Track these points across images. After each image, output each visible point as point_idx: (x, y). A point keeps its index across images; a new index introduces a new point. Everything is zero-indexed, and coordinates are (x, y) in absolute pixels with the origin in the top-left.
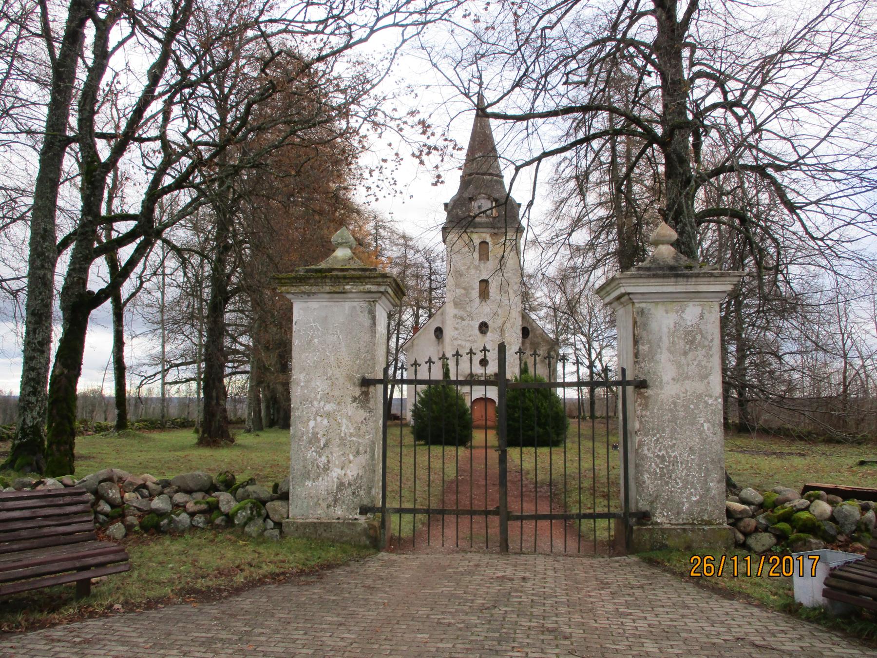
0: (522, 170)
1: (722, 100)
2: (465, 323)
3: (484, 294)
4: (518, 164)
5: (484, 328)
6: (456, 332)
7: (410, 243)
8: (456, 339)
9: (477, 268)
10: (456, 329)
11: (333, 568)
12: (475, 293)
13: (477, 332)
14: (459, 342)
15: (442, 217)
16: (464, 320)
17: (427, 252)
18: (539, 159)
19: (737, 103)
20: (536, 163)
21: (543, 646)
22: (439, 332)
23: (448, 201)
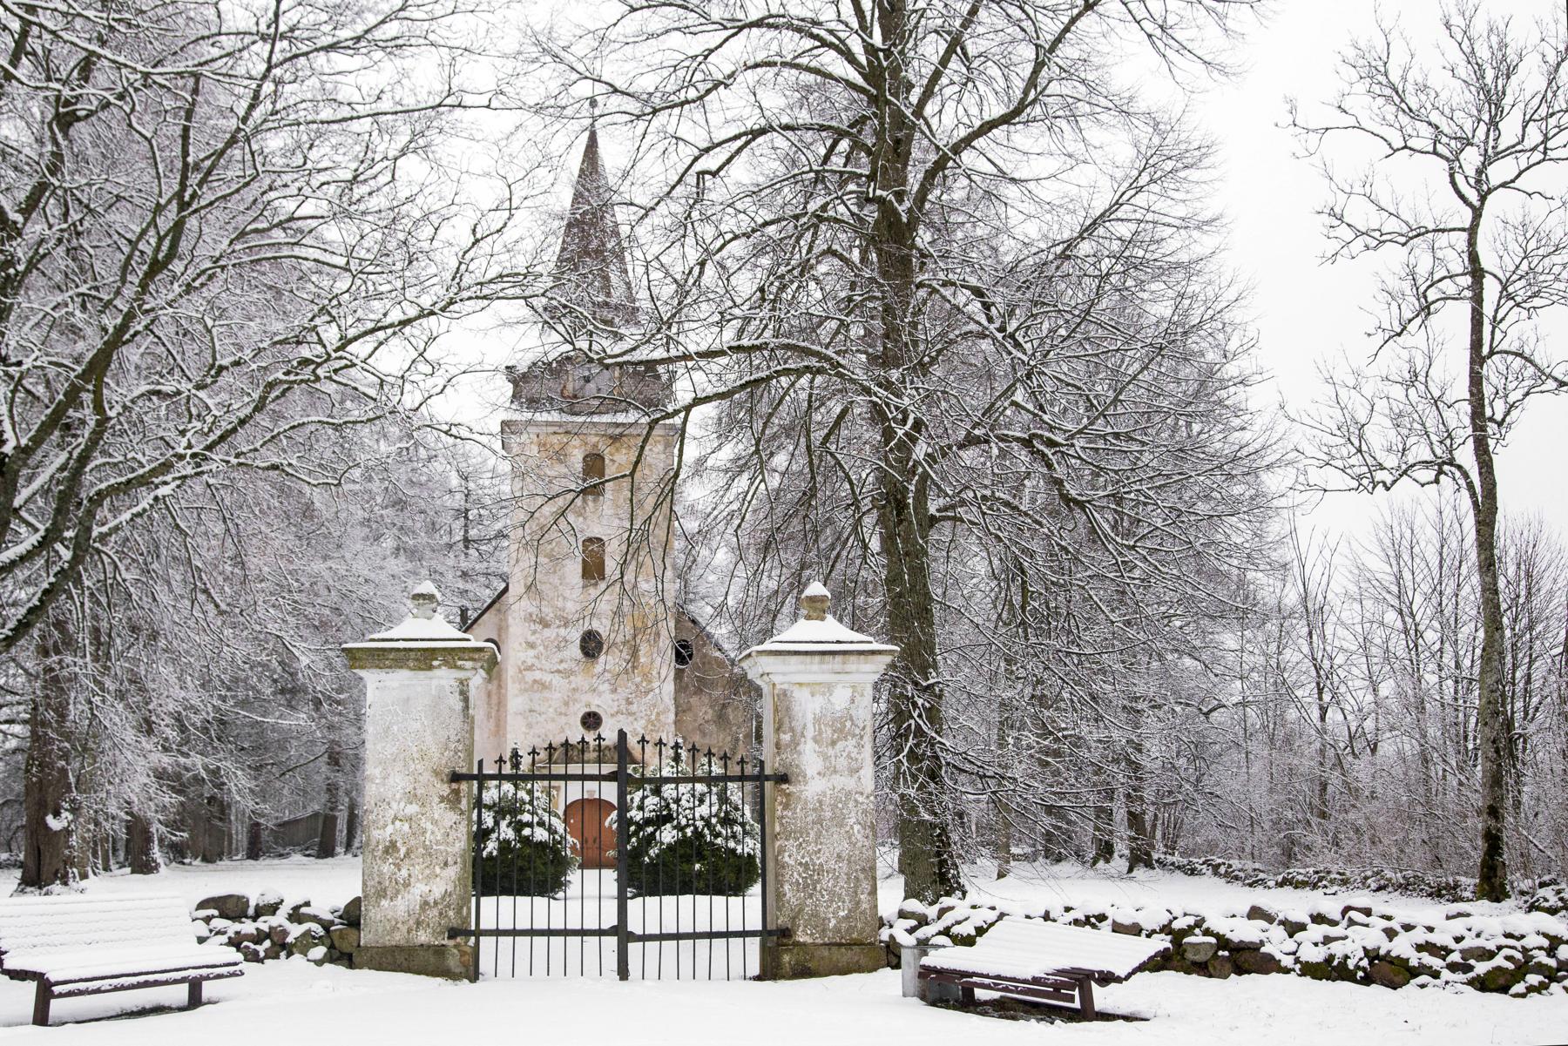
6: (532, 653)
8: (530, 668)
10: (532, 646)
12: (574, 569)
14: (538, 675)
16: (546, 625)
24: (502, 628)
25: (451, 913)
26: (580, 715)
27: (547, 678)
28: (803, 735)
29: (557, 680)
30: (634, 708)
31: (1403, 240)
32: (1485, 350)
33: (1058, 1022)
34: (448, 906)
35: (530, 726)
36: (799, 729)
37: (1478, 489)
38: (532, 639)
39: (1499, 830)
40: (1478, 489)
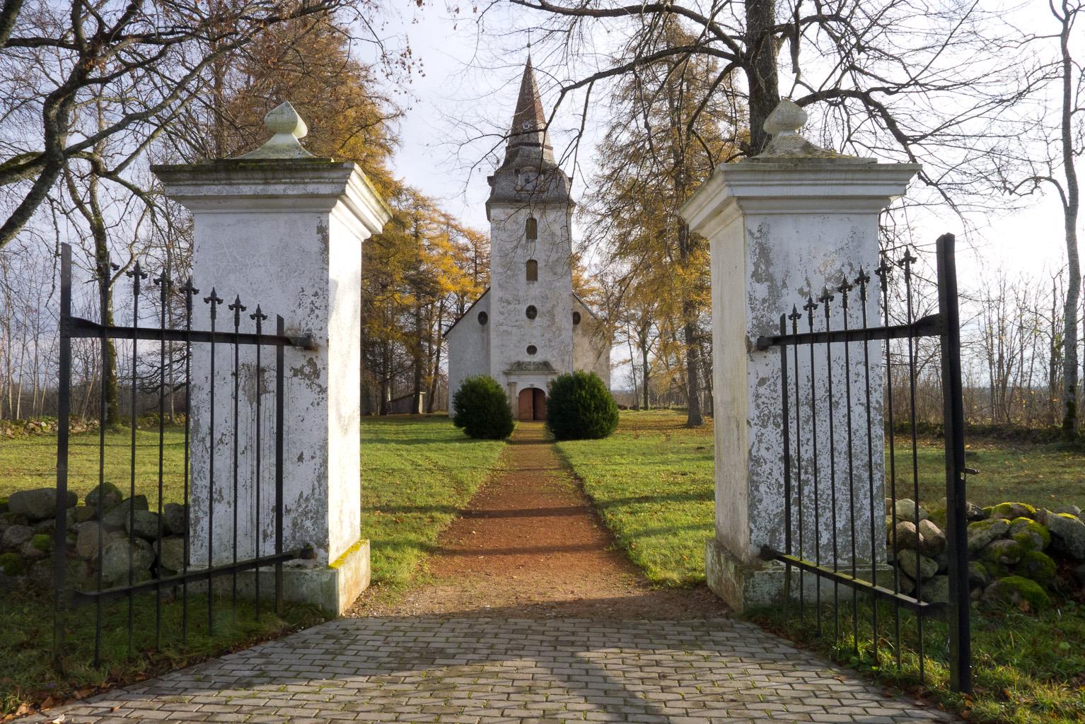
0: (569, 93)
1: (815, 13)
2: (511, 307)
3: (532, 274)
4: (566, 85)
5: (531, 313)
6: (502, 317)
7: (453, 222)
8: (501, 325)
9: (524, 247)
10: (502, 313)
11: (1049, 432)
12: (522, 277)
13: (525, 316)
14: (505, 328)
15: (486, 192)
16: (509, 303)
17: (469, 234)
18: (591, 80)
19: (836, 17)
20: (586, 87)
21: (586, 679)
22: (483, 318)
23: (492, 174)
24: (488, 306)
25: (308, 524)
26: (536, 306)
27: (510, 329)
28: (784, 285)
29: (514, 330)
30: (553, 344)
31: (1017, 44)
32: (1072, 109)
33: (110, 309)
34: (305, 513)
35: (502, 352)
36: (779, 277)
37: (1068, 200)
38: (502, 310)
39: (1075, 400)
40: (1068, 200)
